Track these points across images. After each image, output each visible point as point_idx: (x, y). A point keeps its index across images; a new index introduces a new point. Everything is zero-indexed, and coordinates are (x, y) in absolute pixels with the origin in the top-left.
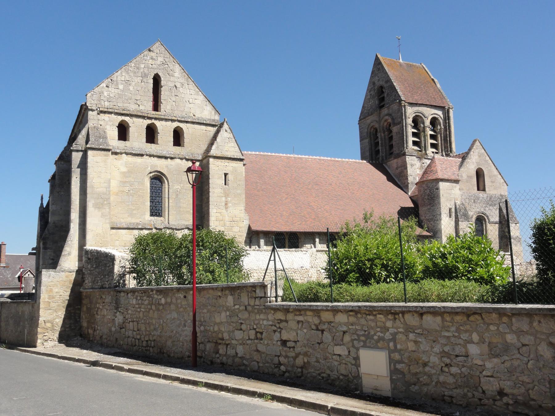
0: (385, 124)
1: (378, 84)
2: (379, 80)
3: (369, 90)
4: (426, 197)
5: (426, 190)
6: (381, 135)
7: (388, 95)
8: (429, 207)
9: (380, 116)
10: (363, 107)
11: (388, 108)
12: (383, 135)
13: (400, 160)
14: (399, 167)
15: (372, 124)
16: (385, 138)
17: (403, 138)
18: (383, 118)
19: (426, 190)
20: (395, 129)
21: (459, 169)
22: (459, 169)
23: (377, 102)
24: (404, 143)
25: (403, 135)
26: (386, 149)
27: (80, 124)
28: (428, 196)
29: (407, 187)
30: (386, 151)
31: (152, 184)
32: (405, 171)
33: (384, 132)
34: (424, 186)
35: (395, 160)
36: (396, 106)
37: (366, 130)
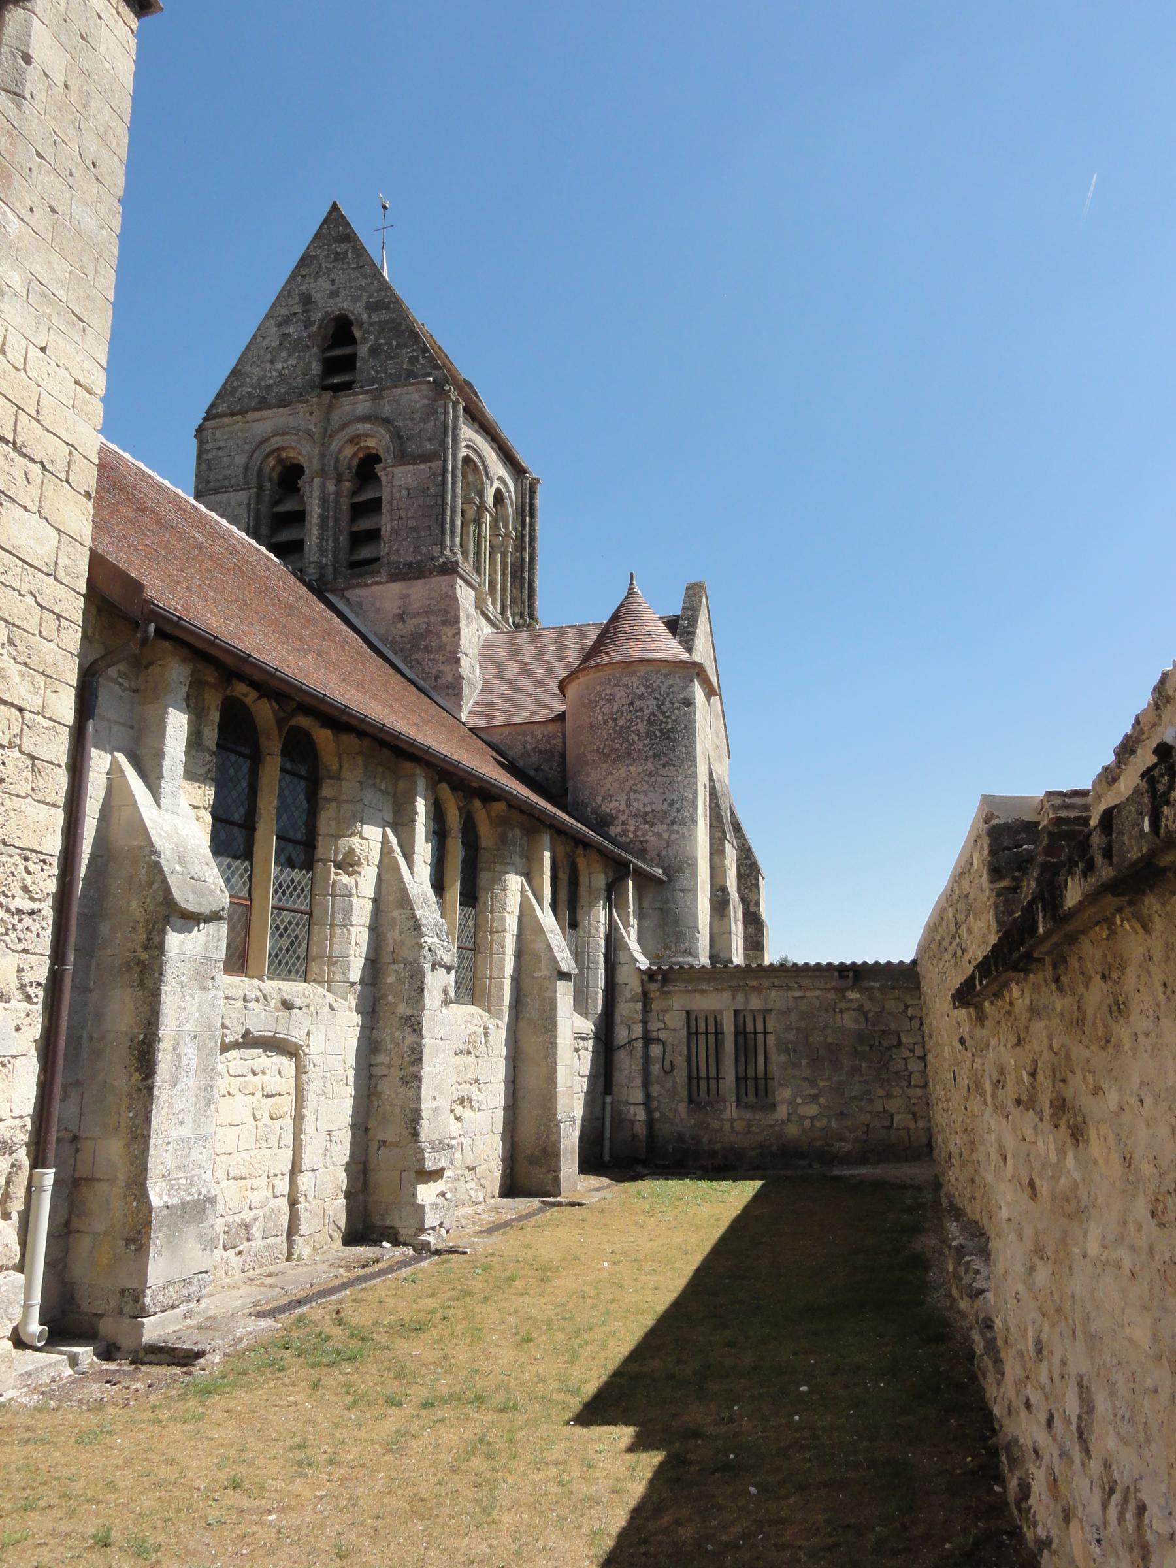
0: (349, 451)
1: (327, 305)
2: (334, 294)
3: (278, 317)
4: (642, 726)
5: (641, 697)
6: (323, 487)
7: (374, 351)
8: (650, 765)
9: (327, 418)
10: (235, 373)
11: (377, 397)
12: (331, 487)
13: (419, 591)
14: (414, 615)
15: (277, 442)
16: (336, 502)
17: (443, 514)
18: (344, 426)
19: (641, 697)
20: (398, 480)
21: (159, 806)
22: (159, 806)
23: (316, 367)
24: (443, 532)
25: (444, 504)
26: (336, 540)
27: (82, 989)
28: (650, 722)
29: (454, 688)
30: (336, 549)
31: (557, 1180)
32: (448, 631)
33: (339, 480)
34: (634, 680)
35: (396, 587)
36: (416, 397)
37: (241, 459)
